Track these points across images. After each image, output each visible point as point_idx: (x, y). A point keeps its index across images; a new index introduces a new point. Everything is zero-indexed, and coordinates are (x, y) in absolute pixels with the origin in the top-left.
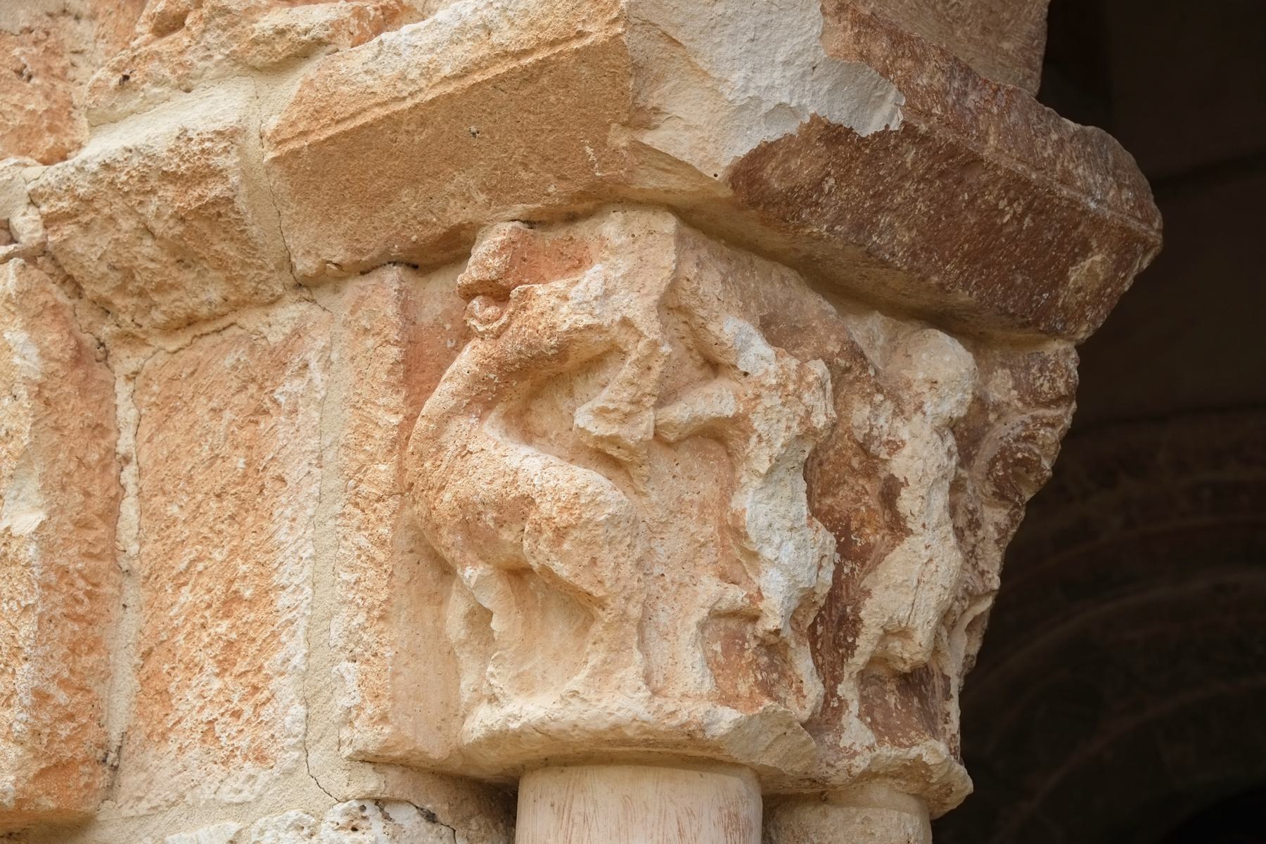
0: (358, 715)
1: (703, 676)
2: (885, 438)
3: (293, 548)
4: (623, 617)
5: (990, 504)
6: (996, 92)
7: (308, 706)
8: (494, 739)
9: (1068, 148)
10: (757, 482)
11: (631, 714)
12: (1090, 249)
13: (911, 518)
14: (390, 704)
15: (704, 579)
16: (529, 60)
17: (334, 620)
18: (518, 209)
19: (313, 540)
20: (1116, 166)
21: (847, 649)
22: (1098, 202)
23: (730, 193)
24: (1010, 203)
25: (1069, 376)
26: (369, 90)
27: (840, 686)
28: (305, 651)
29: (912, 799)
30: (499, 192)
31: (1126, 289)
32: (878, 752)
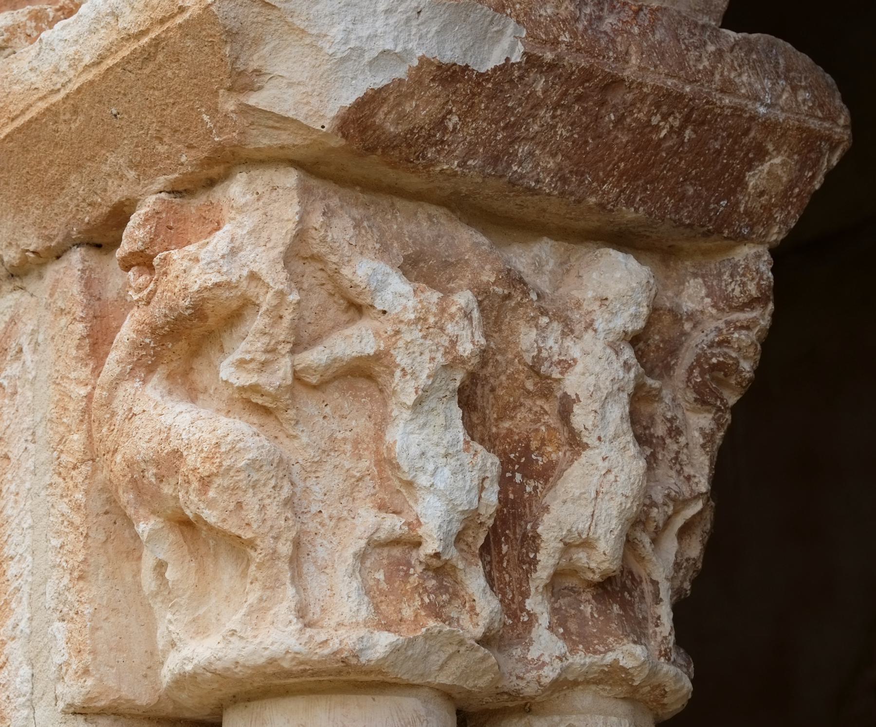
0: (67, 670)
1: (359, 604)
2: (556, 358)
3: (17, 521)
4: (274, 555)
5: (694, 411)
6: (637, 13)
7: (33, 667)
8: (181, 681)
9: (728, 57)
10: (407, 414)
11: (284, 647)
12: (767, 153)
13: (585, 433)
14: (90, 658)
15: (362, 512)
16: (145, 40)
17: (49, 584)
18: (161, 181)
19: (32, 512)
20: (788, 70)
21: (530, 565)
22: (768, 106)
23: (343, 142)
24: (665, 118)
25: (761, 278)
26: (33, 87)
27: (528, 601)
28: (28, 615)
29: (620, 702)
30: (144, 166)
31: (817, 187)
32: (571, 660)
